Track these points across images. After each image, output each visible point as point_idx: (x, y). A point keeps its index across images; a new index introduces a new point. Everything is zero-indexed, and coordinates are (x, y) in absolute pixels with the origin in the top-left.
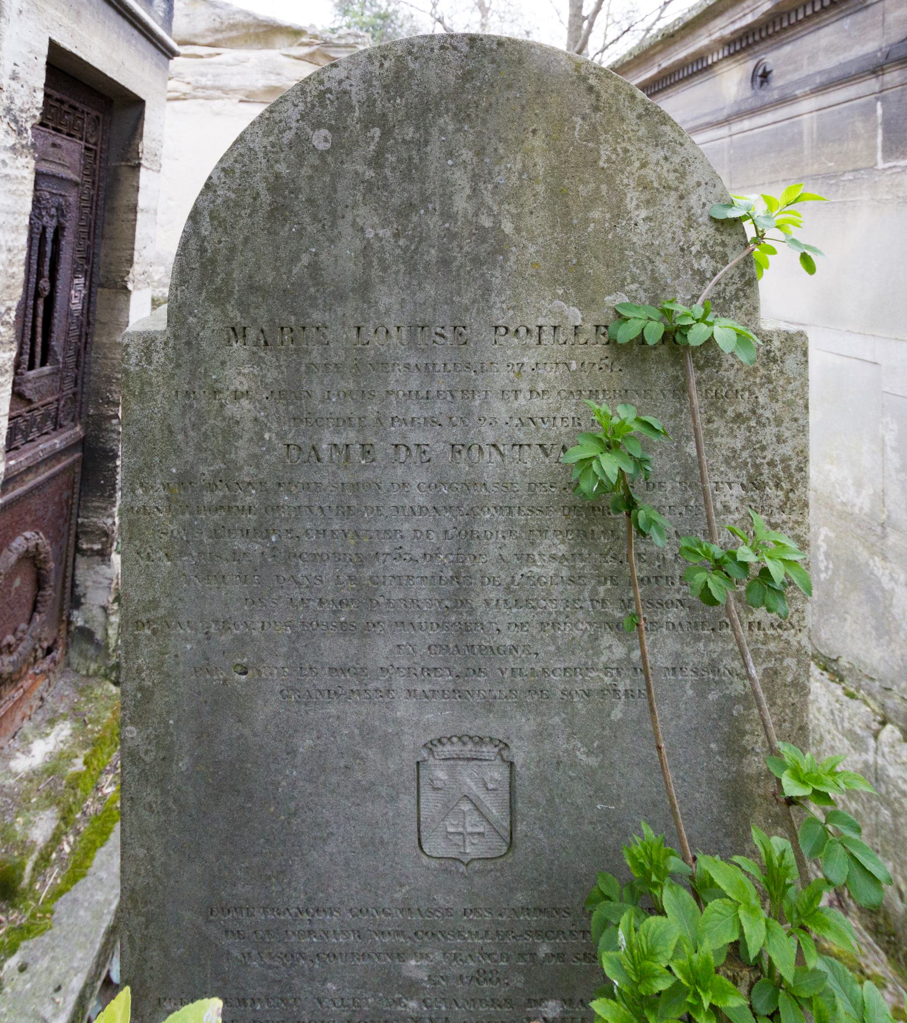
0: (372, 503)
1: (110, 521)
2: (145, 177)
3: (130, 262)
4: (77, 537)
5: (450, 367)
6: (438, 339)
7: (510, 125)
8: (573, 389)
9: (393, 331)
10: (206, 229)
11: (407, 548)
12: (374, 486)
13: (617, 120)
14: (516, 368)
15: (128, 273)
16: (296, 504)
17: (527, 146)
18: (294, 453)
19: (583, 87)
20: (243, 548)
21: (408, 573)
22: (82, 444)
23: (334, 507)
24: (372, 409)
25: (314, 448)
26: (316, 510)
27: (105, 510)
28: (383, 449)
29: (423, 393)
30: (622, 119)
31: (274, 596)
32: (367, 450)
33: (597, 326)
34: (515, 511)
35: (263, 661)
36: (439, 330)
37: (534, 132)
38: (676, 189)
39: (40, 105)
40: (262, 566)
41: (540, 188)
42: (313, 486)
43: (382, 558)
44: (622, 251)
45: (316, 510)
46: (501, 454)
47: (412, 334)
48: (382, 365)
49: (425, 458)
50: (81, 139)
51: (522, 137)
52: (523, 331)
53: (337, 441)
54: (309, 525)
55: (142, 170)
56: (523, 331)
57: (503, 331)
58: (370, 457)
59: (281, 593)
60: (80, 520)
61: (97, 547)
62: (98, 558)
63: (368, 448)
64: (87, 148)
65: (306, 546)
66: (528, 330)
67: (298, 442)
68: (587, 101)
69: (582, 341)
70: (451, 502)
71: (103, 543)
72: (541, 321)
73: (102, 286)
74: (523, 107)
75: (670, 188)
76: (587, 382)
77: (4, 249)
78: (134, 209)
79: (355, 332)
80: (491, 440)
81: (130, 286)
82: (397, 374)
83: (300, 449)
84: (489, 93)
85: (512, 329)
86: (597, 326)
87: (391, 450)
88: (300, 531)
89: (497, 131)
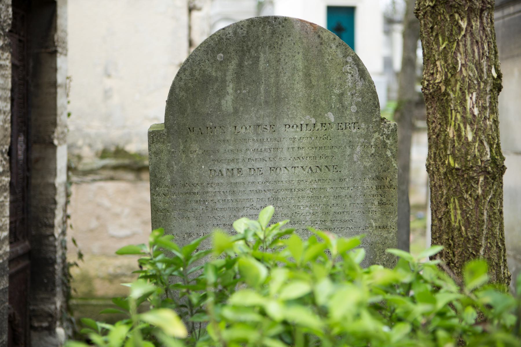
0: (242, 189)
1: (53, 307)
2: (60, 61)
3: (55, 124)
4: (31, 319)
5: (269, 140)
6: (264, 130)
7: (290, 50)
8: (313, 146)
9: (248, 128)
10: (177, 91)
11: (255, 205)
12: (242, 183)
13: (329, 48)
14: (293, 140)
15: (53, 132)
16: (214, 191)
17: (296, 58)
18: (213, 172)
19: (316, 36)
20: (196, 207)
21: (255, 214)
22: (28, 254)
23: (228, 191)
24: (241, 156)
25: (220, 171)
26: (222, 193)
27: (50, 300)
28: (245, 170)
29: (259, 150)
30: (331, 47)
31: (207, 223)
32: (239, 170)
33: (322, 124)
34: (293, 190)
35: (204, 246)
36: (265, 127)
37: (299, 53)
38: (350, 73)
39: (11, 16)
40: (203, 213)
41: (301, 74)
42: (220, 184)
43: (246, 209)
44: (331, 96)
45: (222, 193)
46: (288, 171)
47: (255, 130)
48: (245, 140)
49: (261, 173)
50: (16, 33)
51: (294, 55)
52: (295, 126)
53: (228, 167)
54: (219, 198)
55: (58, 55)
56: (295, 126)
57: (288, 126)
58: (241, 173)
59: (210, 222)
60: (31, 308)
61: (45, 324)
62: (46, 332)
63: (240, 170)
64: (20, 41)
65: (219, 206)
66: (297, 126)
67: (215, 168)
68: (318, 41)
69: (317, 129)
70: (270, 188)
71: (49, 322)
72: (302, 122)
73: (35, 142)
74: (294, 44)
75: (348, 72)
76: (318, 144)
77: (2, 112)
78: (54, 85)
79: (234, 128)
80: (284, 166)
81: (56, 142)
82: (251, 143)
83: (215, 171)
84: (282, 39)
85: (291, 126)
86: (322, 124)
87: (248, 170)
88: (216, 201)
89: (285, 53)
